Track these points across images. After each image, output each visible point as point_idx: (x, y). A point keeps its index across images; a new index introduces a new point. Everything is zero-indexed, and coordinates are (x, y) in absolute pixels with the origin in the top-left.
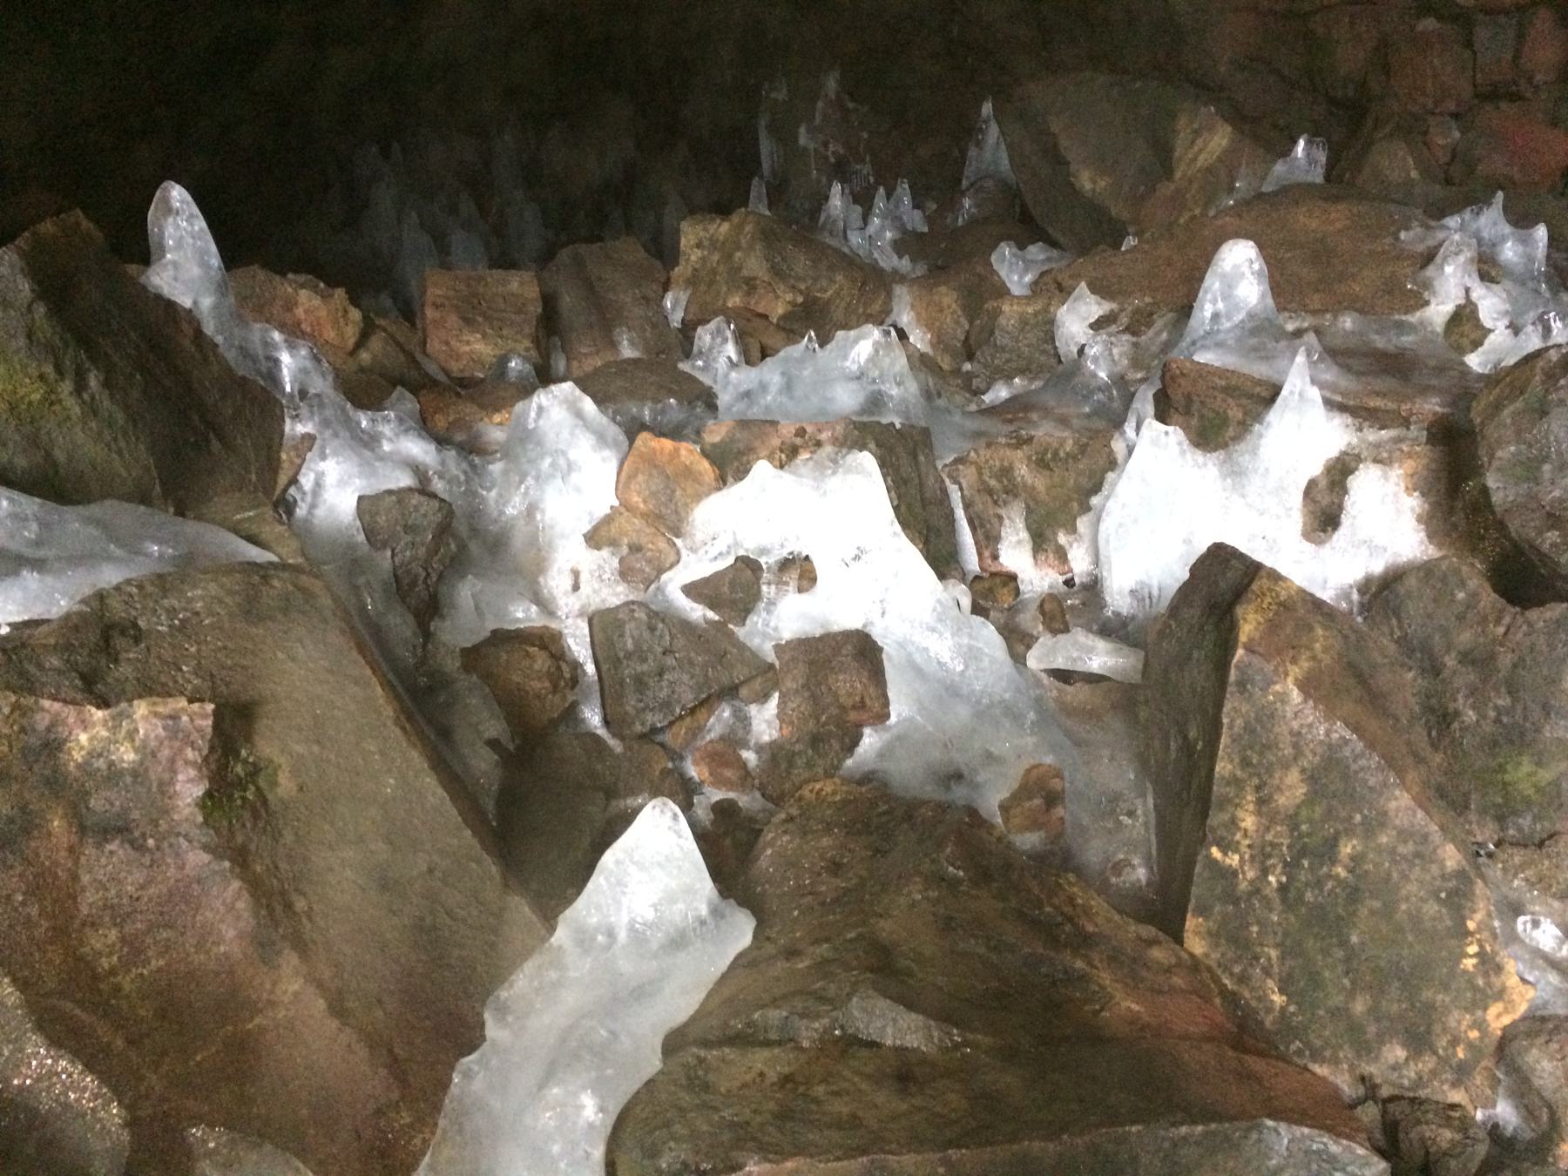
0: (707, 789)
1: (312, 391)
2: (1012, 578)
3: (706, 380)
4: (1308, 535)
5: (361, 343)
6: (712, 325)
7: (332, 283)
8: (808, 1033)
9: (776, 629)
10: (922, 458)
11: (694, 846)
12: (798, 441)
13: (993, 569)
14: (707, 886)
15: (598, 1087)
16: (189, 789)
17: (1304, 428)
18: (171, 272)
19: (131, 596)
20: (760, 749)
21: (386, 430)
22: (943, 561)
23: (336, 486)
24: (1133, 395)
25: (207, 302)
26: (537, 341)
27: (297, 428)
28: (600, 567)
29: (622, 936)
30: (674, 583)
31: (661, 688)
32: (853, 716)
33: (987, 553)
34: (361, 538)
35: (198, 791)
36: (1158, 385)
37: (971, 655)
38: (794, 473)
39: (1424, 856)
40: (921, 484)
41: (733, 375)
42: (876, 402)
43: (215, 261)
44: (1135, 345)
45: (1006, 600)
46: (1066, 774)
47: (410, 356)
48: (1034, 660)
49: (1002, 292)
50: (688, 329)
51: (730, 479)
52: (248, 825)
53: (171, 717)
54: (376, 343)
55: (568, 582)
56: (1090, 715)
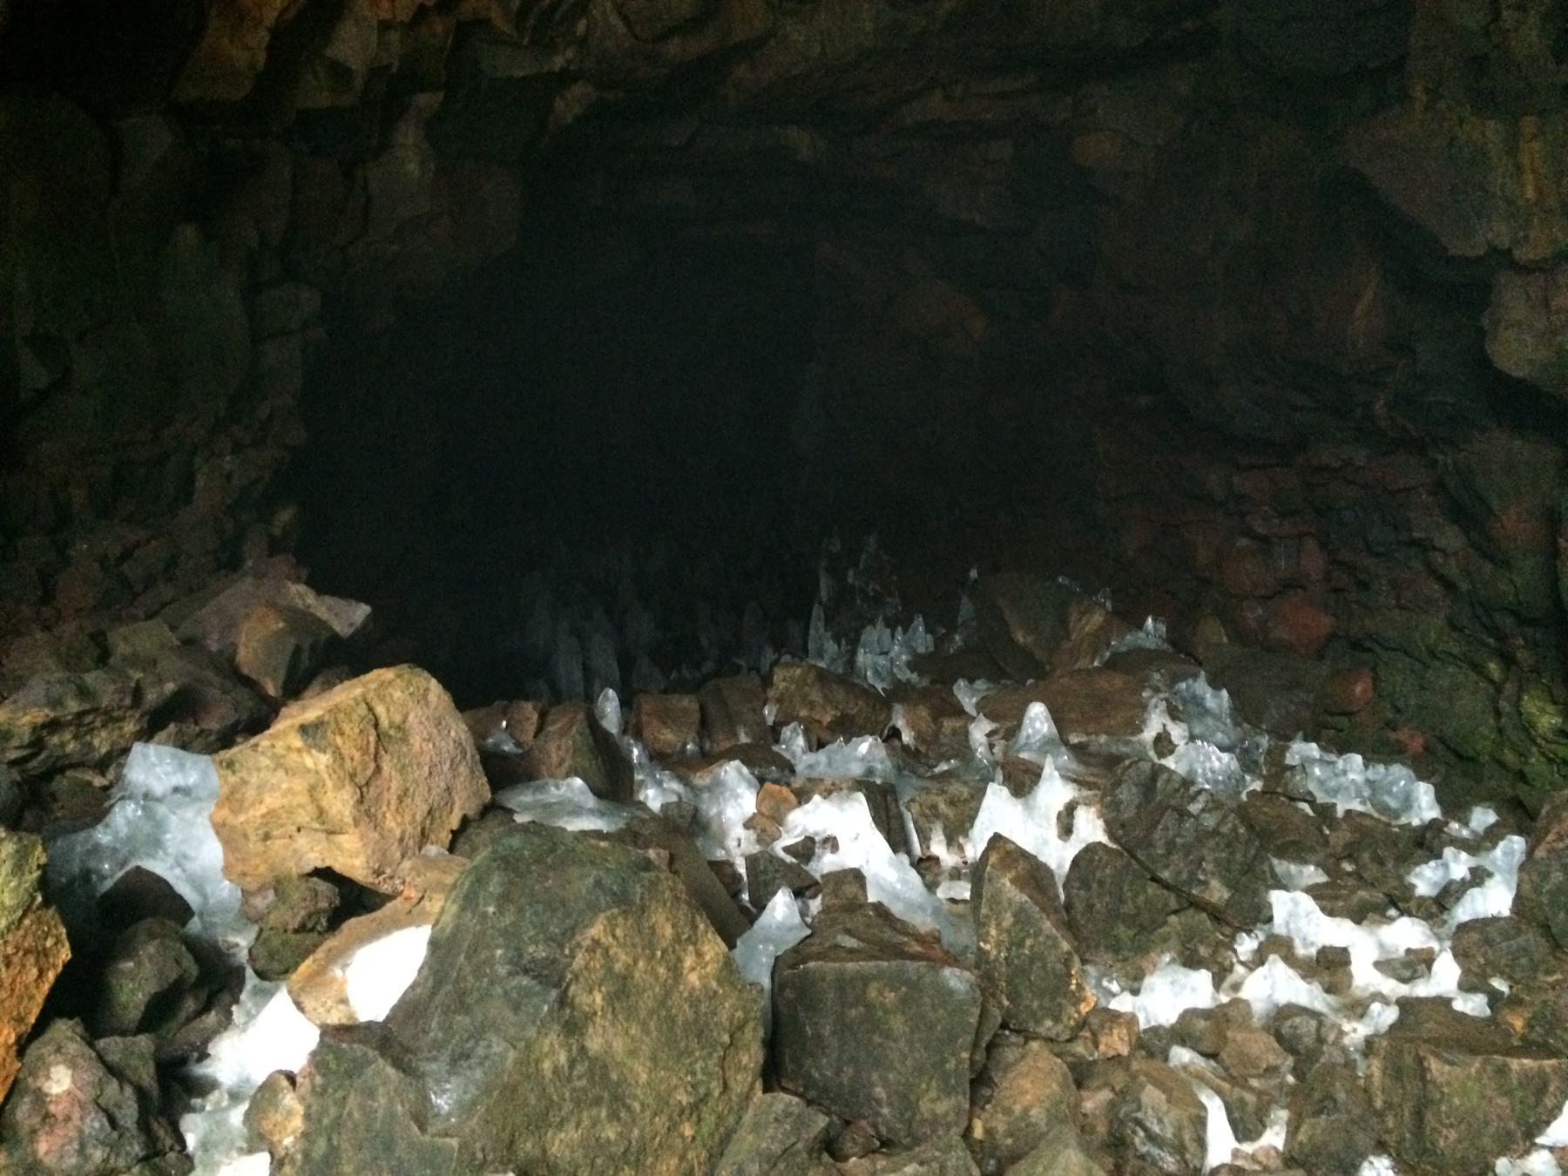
2: (936, 860)
3: (787, 756)
4: (1060, 837)
6: (792, 725)
17: (1054, 791)
22: (898, 842)
26: (698, 733)
27: (638, 777)
30: (778, 848)
37: (904, 882)
39: (1056, 946)
42: (870, 772)
45: (935, 870)
48: (942, 893)
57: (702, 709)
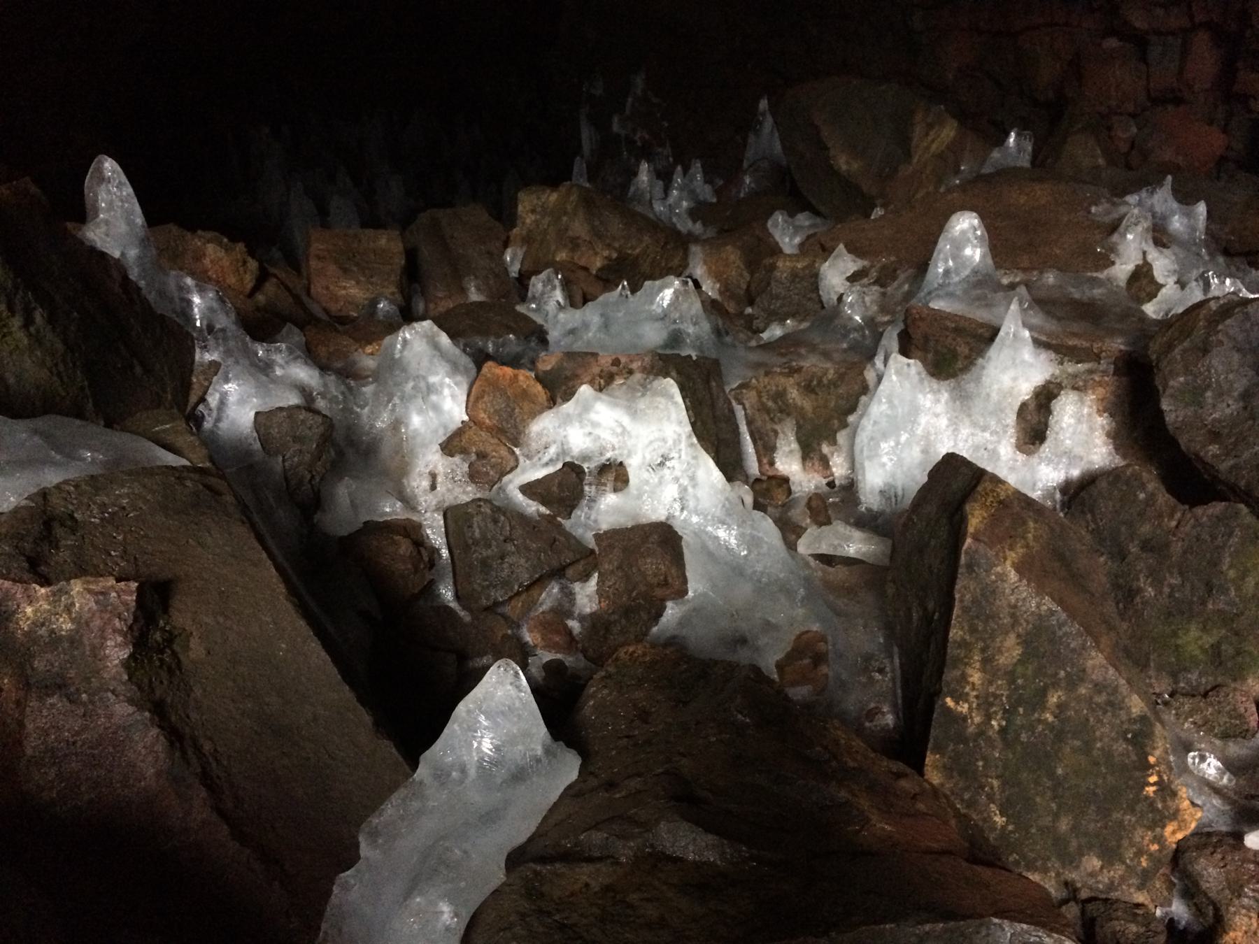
0: (539, 652)
1: (218, 326)
2: (785, 481)
5: (257, 288)
6: (543, 276)
7: (233, 240)
8: (625, 851)
9: (596, 521)
10: (714, 384)
11: (532, 698)
12: (614, 369)
13: (770, 473)
14: (541, 730)
15: (452, 897)
16: (116, 652)
18: (103, 229)
19: (69, 493)
20: (582, 619)
21: (278, 358)
22: (731, 467)
23: (236, 404)
24: (882, 334)
25: (133, 253)
28: (453, 470)
29: (472, 772)
31: (502, 570)
32: (659, 592)
33: (765, 461)
34: (257, 446)
35: (124, 654)
36: (901, 326)
37: (752, 542)
38: (610, 395)
39: (1115, 705)
40: (713, 406)
41: (562, 316)
42: (676, 338)
43: (139, 220)
44: (884, 294)
45: (781, 498)
46: (830, 638)
47: (297, 299)
48: (803, 547)
49: (776, 251)
50: (523, 280)
51: (559, 400)
52: (165, 682)
53: (102, 593)
54: (270, 287)
55: (426, 484)
56: (848, 591)
57: (411, 255)
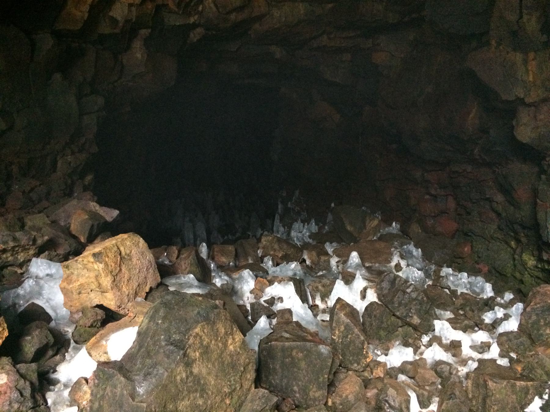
2: (317, 306)
3: (266, 268)
4: (361, 299)
17: (360, 283)
22: (304, 300)
27: (213, 274)
30: (262, 300)
37: (306, 314)
39: (359, 338)
41: (272, 269)
42: (295, 274)
48: (319, 318)
